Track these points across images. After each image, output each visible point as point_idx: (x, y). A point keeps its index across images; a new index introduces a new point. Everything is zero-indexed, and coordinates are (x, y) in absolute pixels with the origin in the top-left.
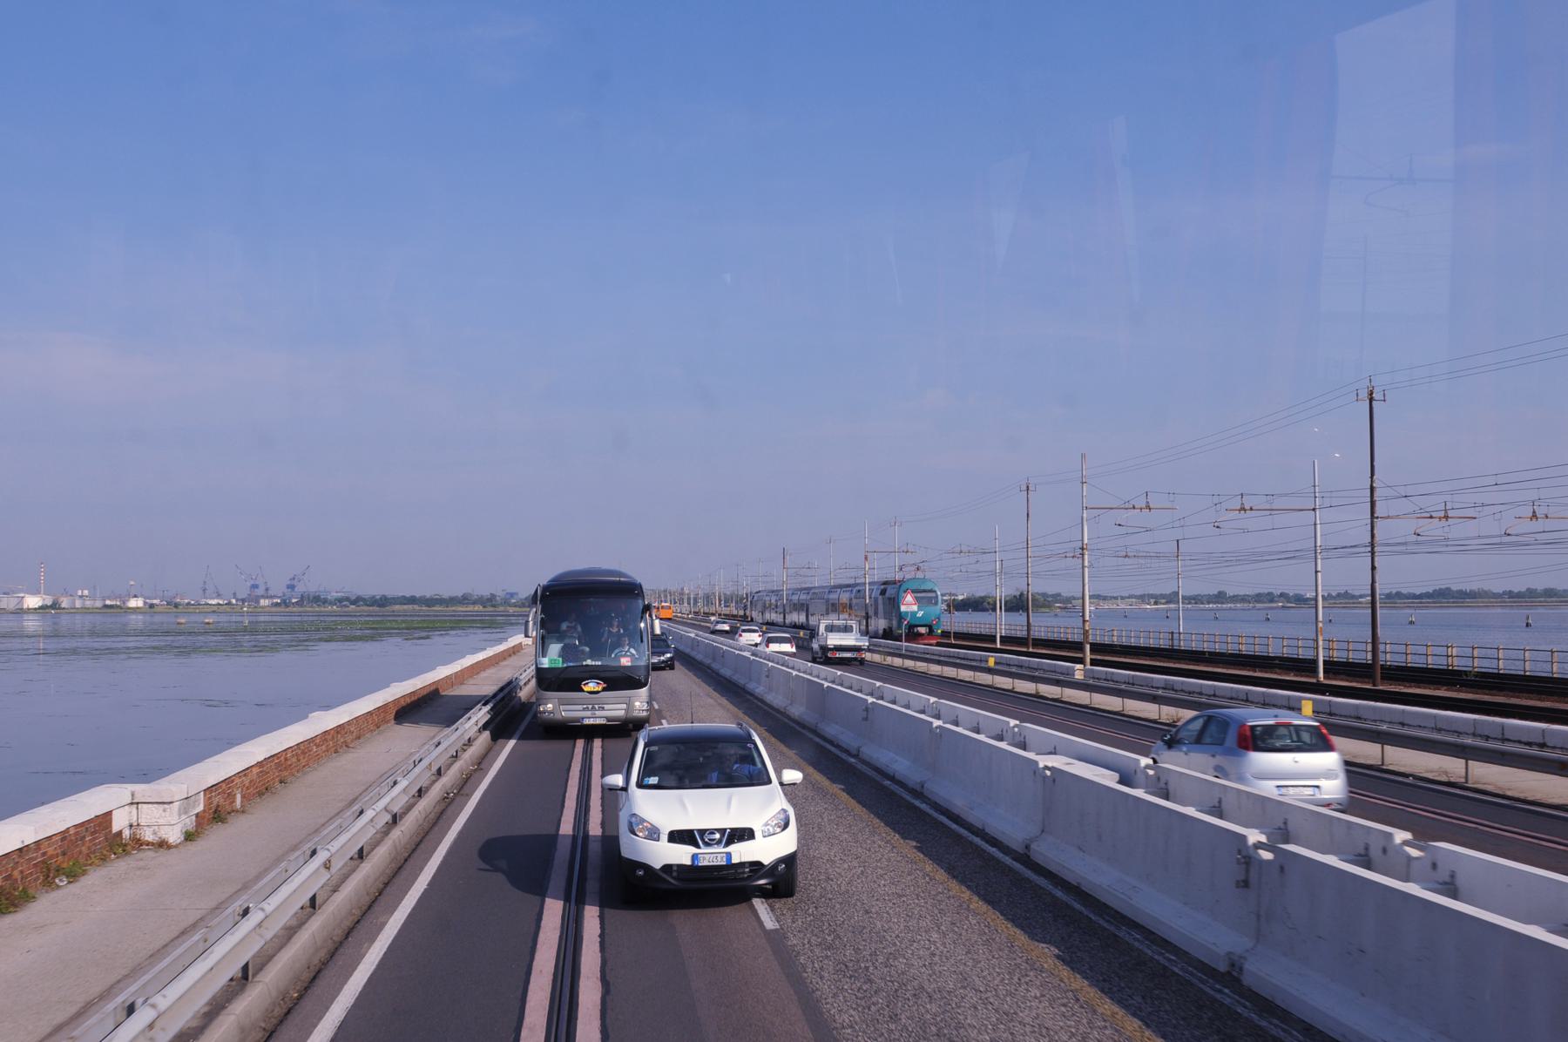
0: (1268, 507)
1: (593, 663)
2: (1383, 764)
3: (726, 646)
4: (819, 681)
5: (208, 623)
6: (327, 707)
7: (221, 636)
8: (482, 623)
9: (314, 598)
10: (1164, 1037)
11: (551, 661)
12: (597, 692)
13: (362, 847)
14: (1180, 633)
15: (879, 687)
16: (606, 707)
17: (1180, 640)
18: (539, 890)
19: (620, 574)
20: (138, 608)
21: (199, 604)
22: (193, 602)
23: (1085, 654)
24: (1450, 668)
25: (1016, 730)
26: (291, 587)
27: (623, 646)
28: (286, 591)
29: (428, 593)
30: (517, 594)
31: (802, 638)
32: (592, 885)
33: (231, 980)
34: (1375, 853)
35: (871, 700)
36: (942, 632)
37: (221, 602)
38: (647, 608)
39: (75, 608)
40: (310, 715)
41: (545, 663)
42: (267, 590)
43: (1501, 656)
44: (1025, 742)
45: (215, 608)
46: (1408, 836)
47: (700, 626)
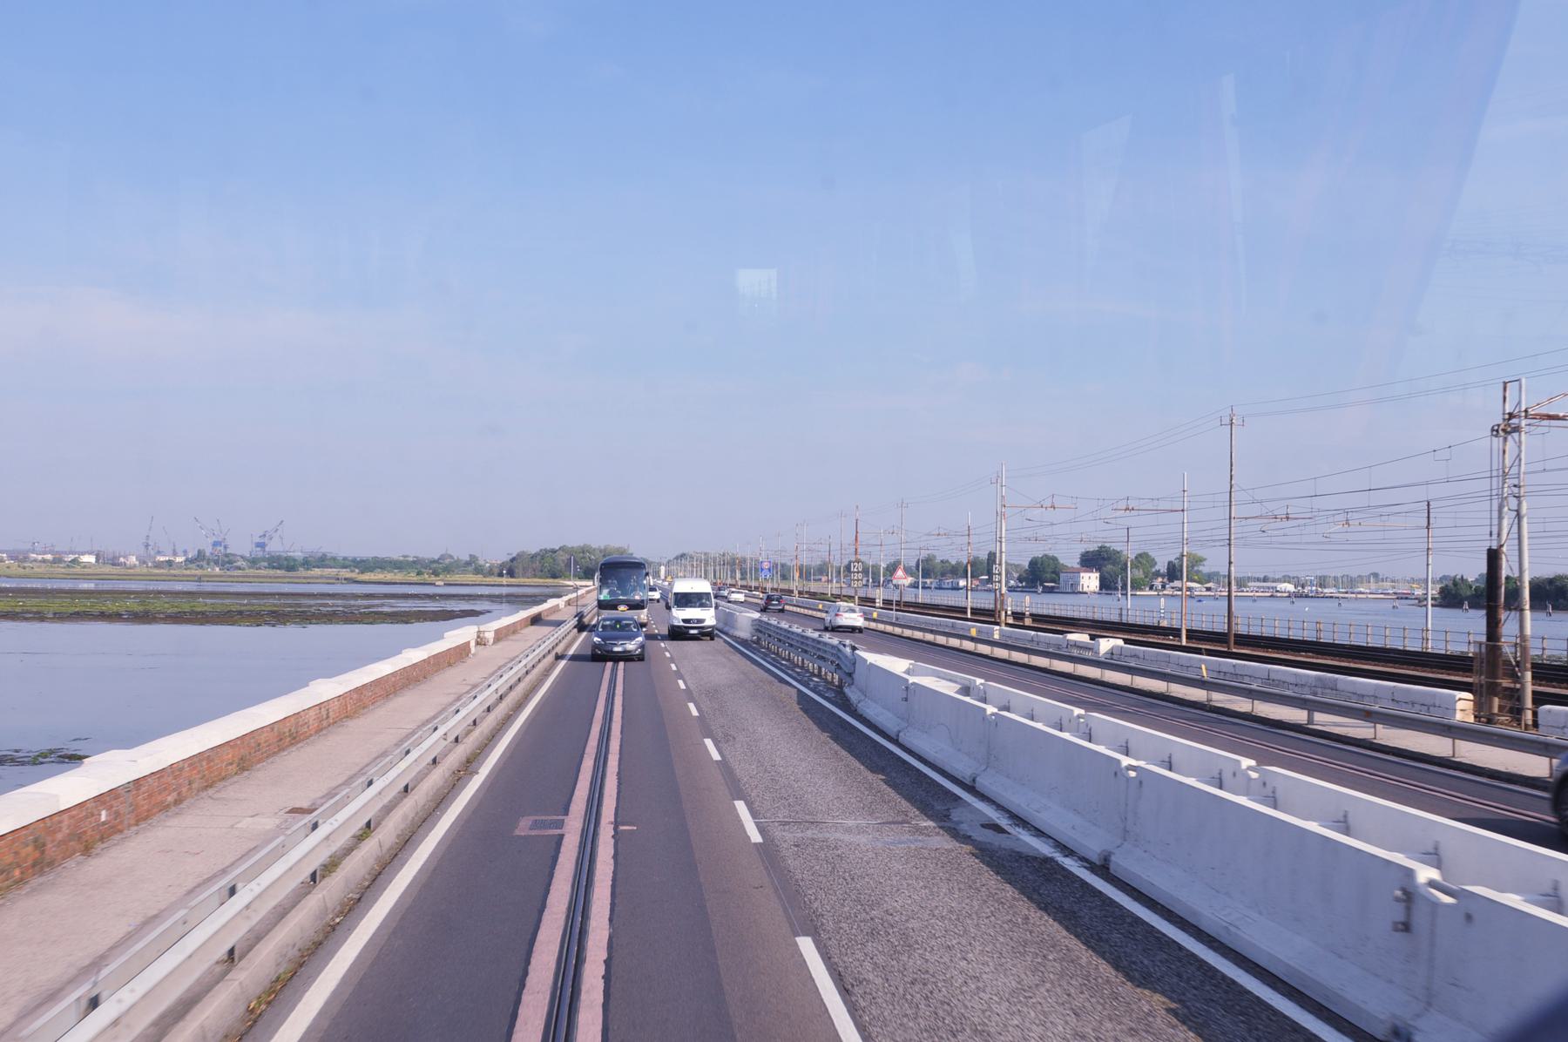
0: (1155, 508)
2: (1453, 756)
6: (330, 674)
14: (1128, 610)
17: (1128, 615)
24: (1424, 650)
25: (982, 687)
33: (302, 883)
34: (1227, 776)
40: (446, 634)
41: (602, 597)
43: (1369, 632)
46: (1253, 763)
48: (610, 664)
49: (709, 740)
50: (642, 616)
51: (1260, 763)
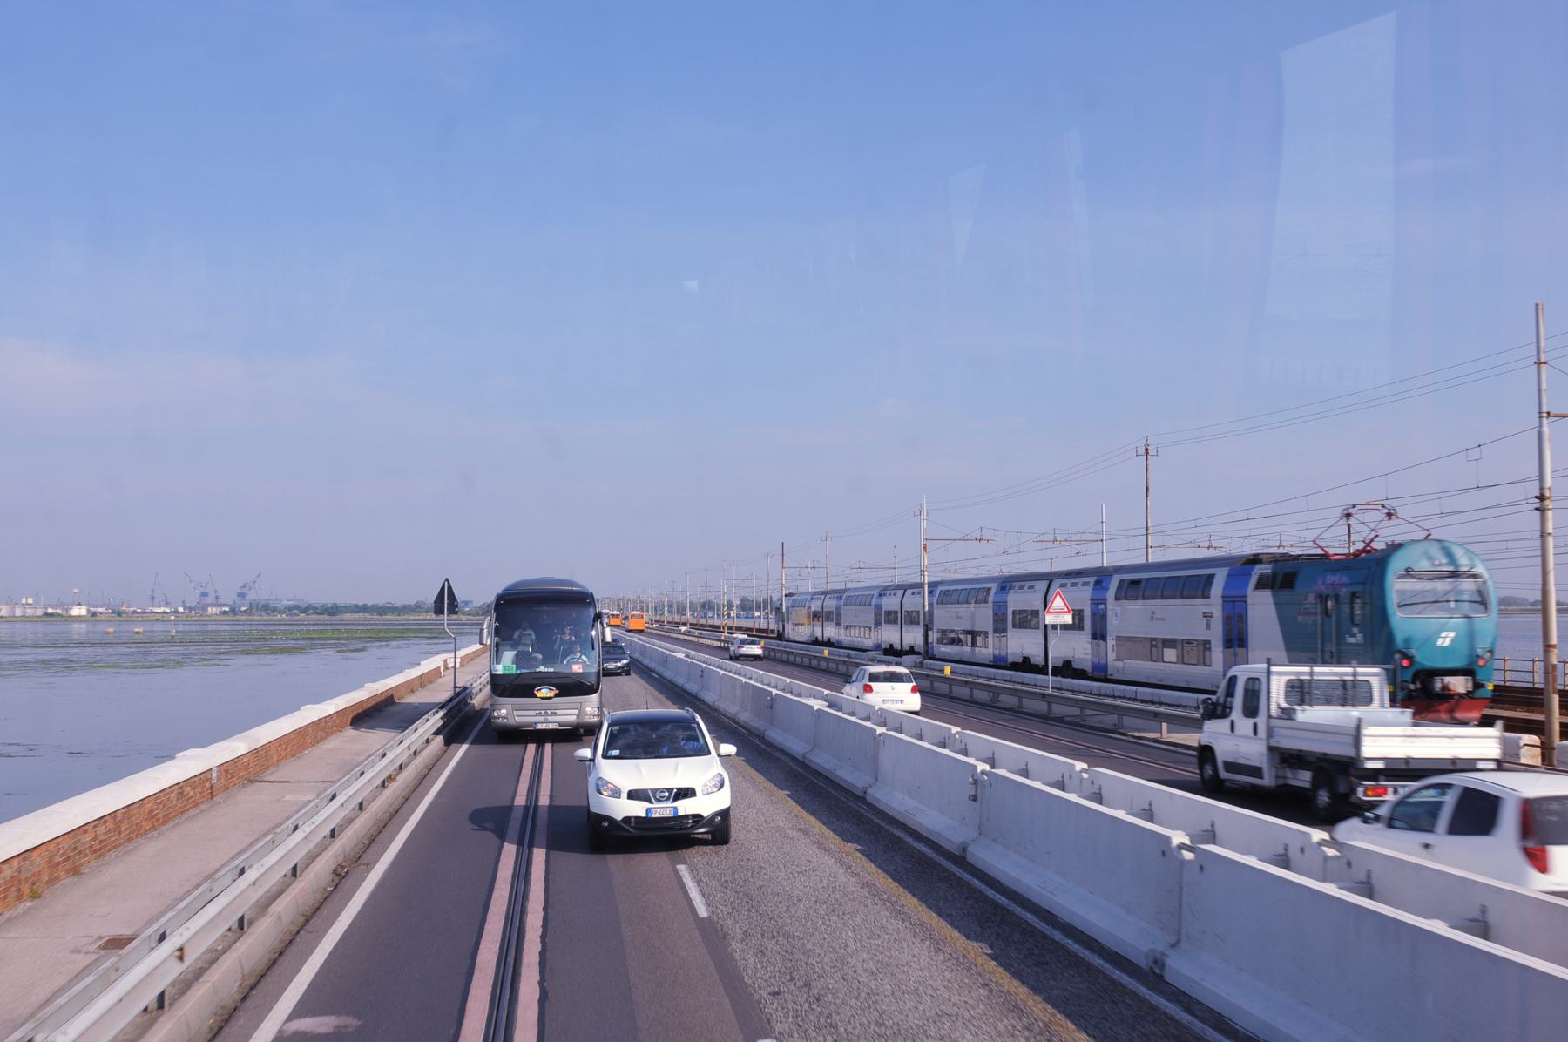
1: (546, 670)
4: (792, 697)
5: (138, 633)
7: (137, 647)
8: (429, 633)
9: (264, 606)
11: (505, 668)
12: (550, 698)
13: (296, 865)
16: (558, 712)
18: (502, 837)
19: (572, 583)
20: (80, 616)
21: (146, 613)
22: (139, 610)
23: (1549, 714)
26: (242, 595)
27: (575, 654)
28: (236, 598)
29: (381, 602)
30: (471, 602)
31: (825, 658)
32: (541, 833)
34: (1294, 853)
36: (1497, 688)
37: (168, 610)
38: (598, 617)
39: (14, 616)
41: (500, 669)
42: (217, 598)
44: (966, 749)
45: (159, 617)
46: (1085, 766)
47: (669, 637)
48: (531, 748)
49: (701, 916)
50: (588, 709)
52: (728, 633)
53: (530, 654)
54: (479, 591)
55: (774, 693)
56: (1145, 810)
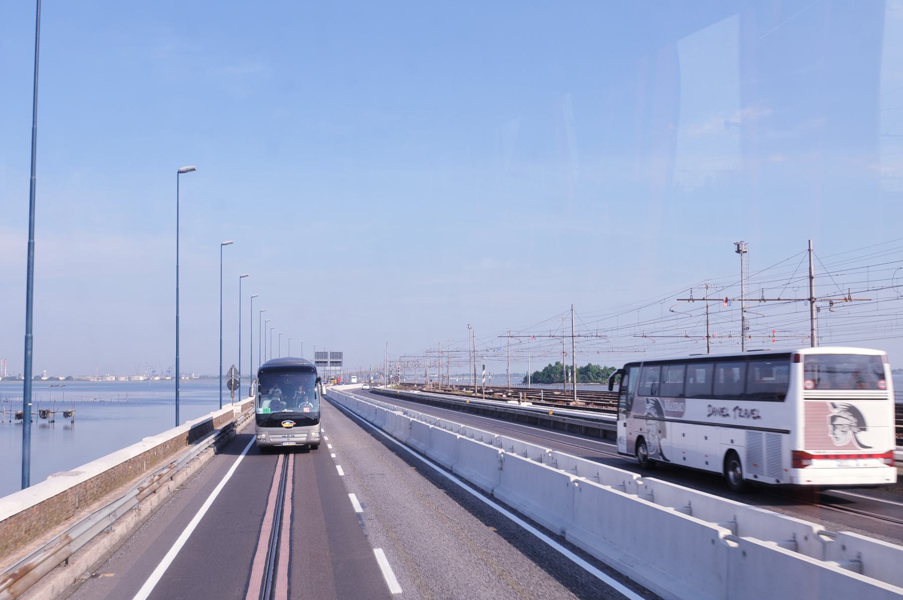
1: (288, 411)
3: (370, 403)
4: (426, 424)
10: (580, 597)
12: (291, 427)
15: (438, 420)
16: (296, 435)
27: (305, 402)
34: (800, 539)
35: (459, 436)
38: (319, 380)
40: (143, 439)
41: (261, 411)
44: (541, 458)
46: (639, 476)
48: (281, 457)
50: (313, 434)
51: (643, 476)
52: (544, 399)
53: (279, 402)
54: (251, 368)
55: (458, 437)
56: (621, 485)
